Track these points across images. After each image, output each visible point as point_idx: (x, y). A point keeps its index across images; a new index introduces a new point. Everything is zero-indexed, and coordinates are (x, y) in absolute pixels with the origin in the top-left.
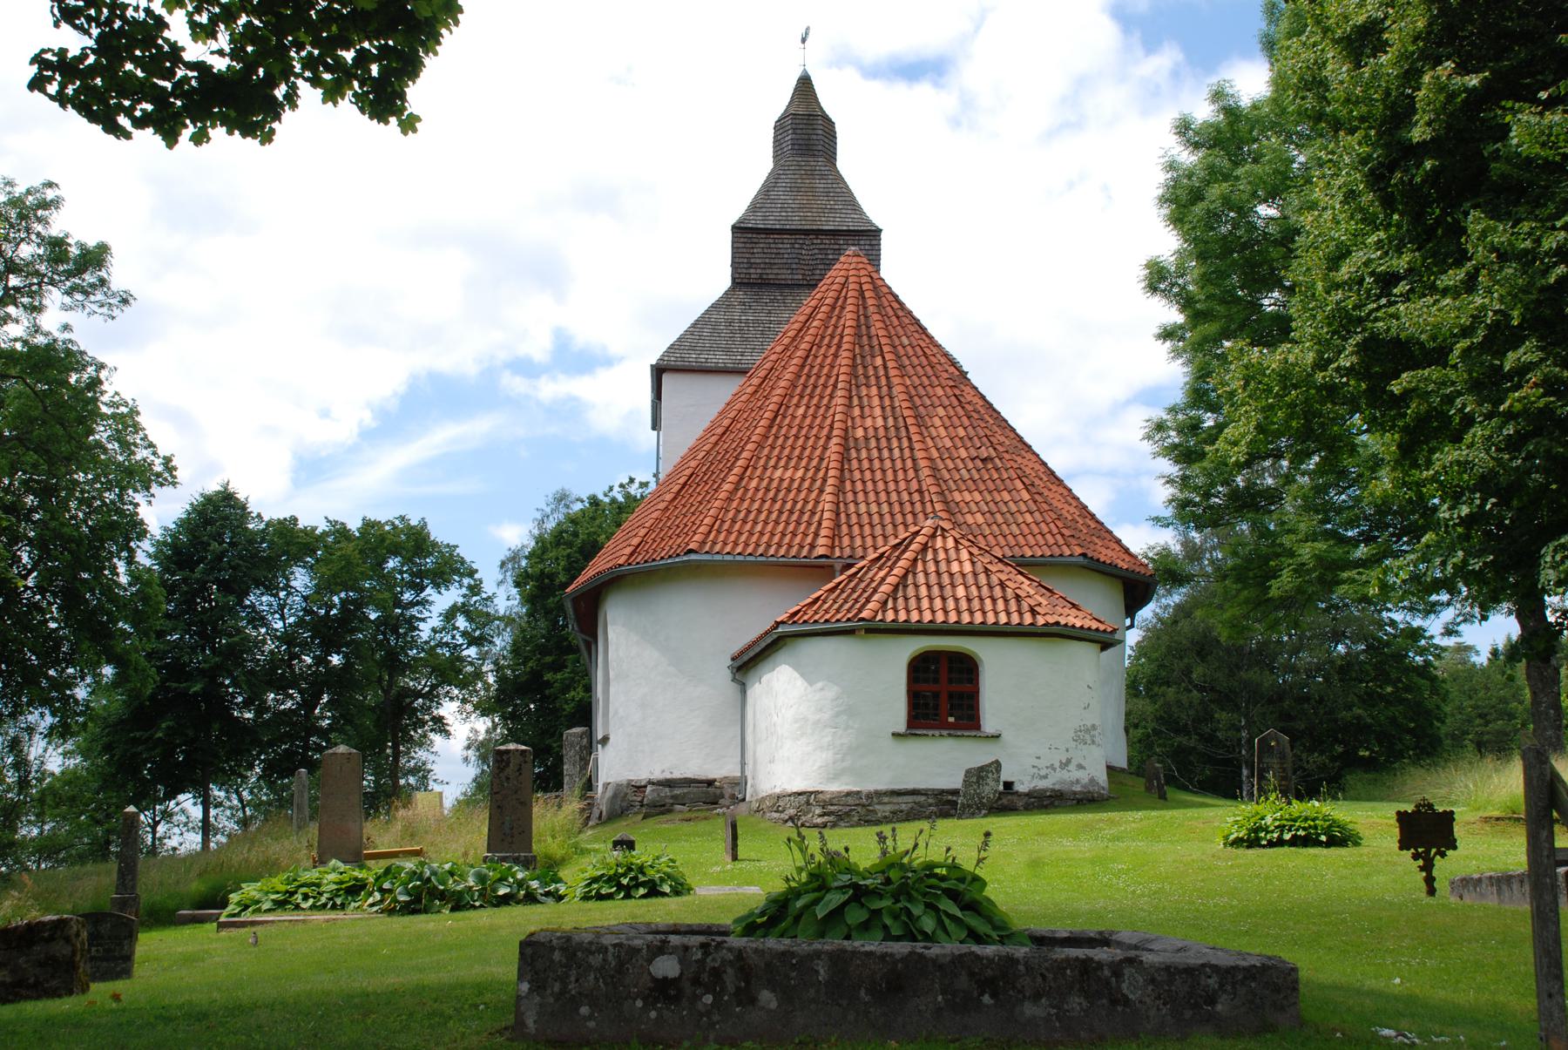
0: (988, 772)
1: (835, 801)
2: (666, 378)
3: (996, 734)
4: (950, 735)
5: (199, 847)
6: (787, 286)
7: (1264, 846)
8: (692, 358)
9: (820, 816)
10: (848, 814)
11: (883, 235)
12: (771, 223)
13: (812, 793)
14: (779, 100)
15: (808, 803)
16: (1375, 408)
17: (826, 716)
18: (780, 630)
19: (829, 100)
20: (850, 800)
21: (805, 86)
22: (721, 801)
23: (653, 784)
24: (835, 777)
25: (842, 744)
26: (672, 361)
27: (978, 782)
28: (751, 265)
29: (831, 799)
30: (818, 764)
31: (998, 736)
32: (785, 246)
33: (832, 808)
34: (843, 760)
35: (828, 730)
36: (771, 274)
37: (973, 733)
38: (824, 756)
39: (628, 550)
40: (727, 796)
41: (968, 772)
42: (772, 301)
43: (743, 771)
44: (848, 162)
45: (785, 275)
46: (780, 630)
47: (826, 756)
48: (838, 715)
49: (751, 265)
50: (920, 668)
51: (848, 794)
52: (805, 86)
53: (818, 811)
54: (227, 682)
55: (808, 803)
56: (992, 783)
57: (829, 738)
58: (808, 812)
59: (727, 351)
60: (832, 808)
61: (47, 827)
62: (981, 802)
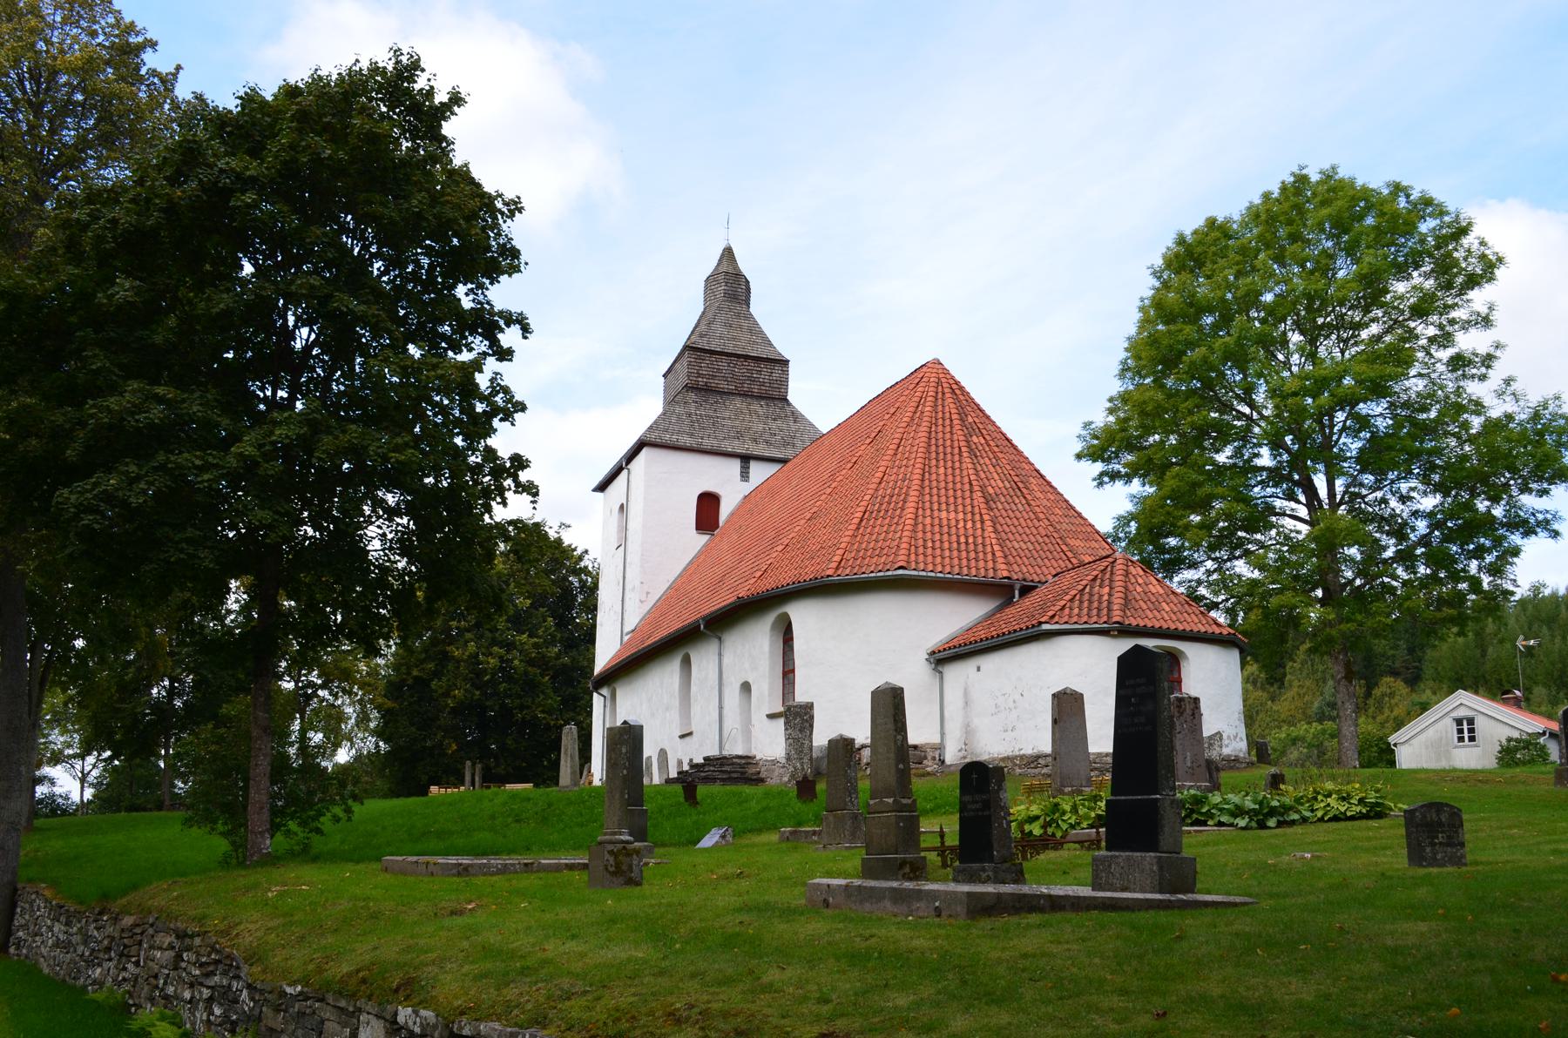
1: (1097, 760)
2: (645, 451)
5: (939, 845)
7: (60, 815)
12: (715, 345)
16: (1457, 403)
19: (745, 266)
21: (728, 253)
22: (925, 762)
26: (653, 437)
28: (699, 375)
32: (723, 364)
36: (713, 383)
39: (834, 565)
40: (929, 758)
42: (716, 402)
43: (943, 734)
44: (757, 308)
45: (723, 385)
49: (699, 375)
52: (728, 253)
54: (183, 769)
56: (1218, 749)
59: (692, 435)
61: (264, 206)
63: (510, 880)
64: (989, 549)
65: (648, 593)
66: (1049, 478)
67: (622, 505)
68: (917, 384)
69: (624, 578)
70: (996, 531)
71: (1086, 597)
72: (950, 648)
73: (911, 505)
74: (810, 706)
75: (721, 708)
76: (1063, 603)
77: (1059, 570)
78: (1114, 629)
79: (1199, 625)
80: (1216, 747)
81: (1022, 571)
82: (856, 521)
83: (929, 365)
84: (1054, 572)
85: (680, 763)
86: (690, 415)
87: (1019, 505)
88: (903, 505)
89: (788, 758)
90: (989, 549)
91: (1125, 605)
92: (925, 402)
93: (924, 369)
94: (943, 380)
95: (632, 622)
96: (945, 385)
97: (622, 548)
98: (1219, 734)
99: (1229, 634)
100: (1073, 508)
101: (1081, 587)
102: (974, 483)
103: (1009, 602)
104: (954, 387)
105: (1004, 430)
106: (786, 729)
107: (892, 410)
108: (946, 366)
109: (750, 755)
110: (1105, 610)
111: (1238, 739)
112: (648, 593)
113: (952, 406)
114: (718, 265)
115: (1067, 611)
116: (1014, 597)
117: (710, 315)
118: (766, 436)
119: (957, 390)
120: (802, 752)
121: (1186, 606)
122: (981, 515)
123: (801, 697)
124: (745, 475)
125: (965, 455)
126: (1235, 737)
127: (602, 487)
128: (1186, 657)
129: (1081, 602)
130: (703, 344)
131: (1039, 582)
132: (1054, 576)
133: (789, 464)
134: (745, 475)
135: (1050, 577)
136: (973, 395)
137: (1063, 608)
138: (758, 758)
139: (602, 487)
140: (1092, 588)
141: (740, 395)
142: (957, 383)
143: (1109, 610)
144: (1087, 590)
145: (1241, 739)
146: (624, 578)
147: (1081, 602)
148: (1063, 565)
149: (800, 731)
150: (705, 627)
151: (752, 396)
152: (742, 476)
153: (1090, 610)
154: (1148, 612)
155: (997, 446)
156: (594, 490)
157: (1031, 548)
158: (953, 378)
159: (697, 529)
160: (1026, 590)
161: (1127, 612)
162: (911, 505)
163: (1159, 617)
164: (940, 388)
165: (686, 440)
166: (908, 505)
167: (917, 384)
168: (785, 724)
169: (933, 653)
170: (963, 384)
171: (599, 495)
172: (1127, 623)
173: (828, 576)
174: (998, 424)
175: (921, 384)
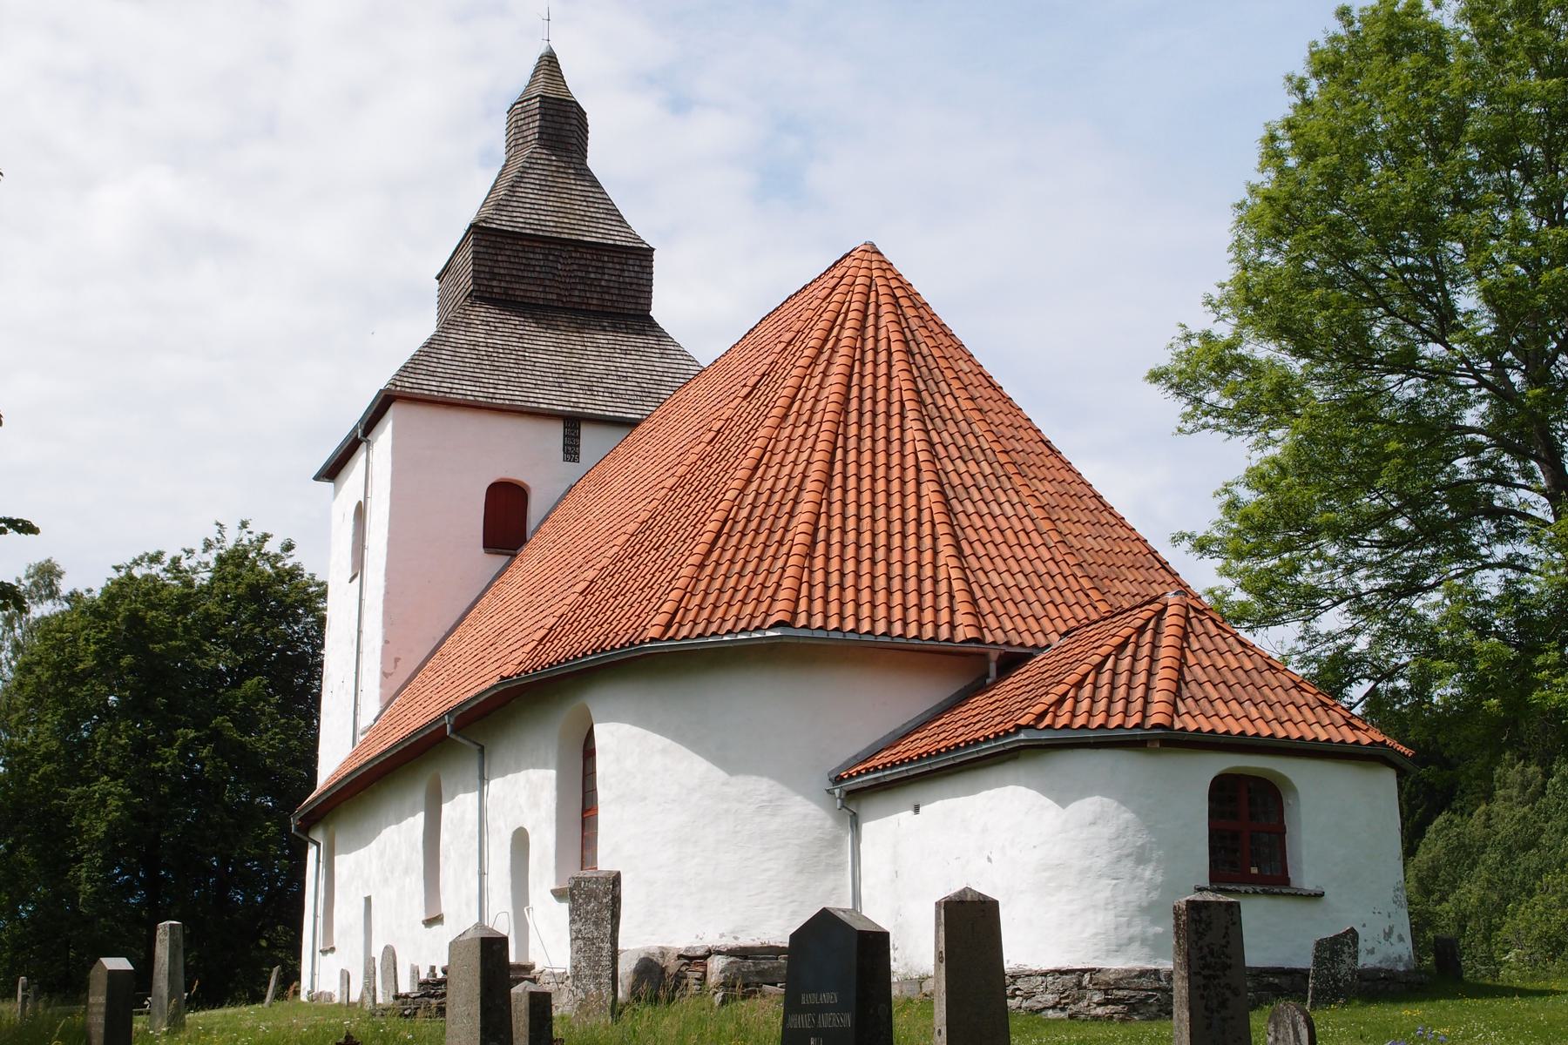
0: (1343, 944)
1: (1123, 984)
3: (1318, 891)
4: (1265, 893)
6: (537, 306)
8: (432, 386)
9: (1099, 1004)
10: (1143, 1001)
11: (656, 255)
13: (1084, 971)
14: (517, 76)
15: (1079, 985)
17: (1101, 862)
18: (1022, 736)
19: (580, 84)
20: (1144, 982)
21: (549, 63)
23: (719, 953)
24: (1119, 949)
25: (1127, 903)
26: (407, 385)
27: (1331, 959)
28: (494, 275)
29: (1116, 981)
30: (1090, 931)
31: (1319, 896)
33: (1120, 993)
34: (1129, 924)
35: (1105, 881)
37: (1284, 891)
38: (1100, 918)
39: (661, 619)
41: (1320, 945)
45: (536, 293)
46: (1022, 736)
47: (1103, 920)
48: (1119, 860)
49: (494, 275)
50: (1224, 791)
51: (1143, 973)
53: (1097, 997)
55: (1079, 985)
56: (1349, 961)
57: (1108, 893)
58: (1080, 999)
59: (476, 381)
60: (1120, 993)
62: (1337, 987)
63: (1444, 1008)
64: (943, 587)
65: (397, 660)
66: (1066, 455)
67: (360, 502)
68: (834, 289)
69: (359, 632)
70: (960, 554)
71: (1105, 678)
72: (902, 762)
73: (805, 508)
74: (616, 880)
75: (482, 874)
76: (1062, 689)
77: (1072, 623)
78: (1153, 739)
79: (1317, 728)
80: (1345, 957)
81: (1003, 630)
82: (708, 537)
83: (856, 254)
84: (1063, 629)
85: (415, 971)
86: (475, 346)
87: (1007, 506)
88: (793, 508)
89: (576, 975)
90: (943, 587)
91: (1178, 693)
92: (845, 320)
93: (848, 262)
94: (880, 281)
95: (366, 720)
96: (881, 290)
97: (357, 580)
98: (1352, 935)
99: (1373, 743)
100: (1108, 509)
101: (1097, 659)
102: (924, 466)
103: (979, 687)
104: (899, 293)
105: (988, 369)
106: (572, 921)
107: (787, 336)
108: (888, 257)
109: (523, 963)
110: (1104, 702)
111: (1394, 939)
112: (397, 660)
113: (893, 327)
114: (531, 83)
115: (1068, 704)
116: (987, 676)
117: (513, 172)
118: (610, 381)
119: (905, 300)
120: (598, 963)
121: (1293, 691)
122: (933, 525)
123: (606, 861)
124: (571, 451)
125: (911, 415)
126: (1388, 935)
127: (333, 471)
128: (1293, 789)
129: (1095, 687)
130: (504, 223)
131: (1035, 646)
132: (1066, 634)
133: (639, 429)
134: (571, 451)
135: (1054, 637)
136: (935, 309)
137: (1062, 699)
138: (538, 968)
139: (333, 471)
140: (1117, 659)
141: (565, 309)
142: (905, 286)
143: (1146, 702)
144: (1109, 665)
145: (1401, 939)
146: (359, 632)
147: (1095, 687)
148: (1081, 615)
149: (595, 923)
150: (452, 732)
151: (587, 313)
152: (566, 452)
153: (1111, 701)
154: (1219, 705)
155: (972, 399)
156: (317, 478)
157: (1024, 584)
158: (898, 277)
159: (485, 546)
160: (1013, 660)
161: (1180, 704)
162: (805, 508)
163: (1240, 714)
164: (873, 294)
165: (467, 390)
166: (800, 508)
167: (834, 289)
168: (571, 911)
169: (838, 780)
170: (916, 288)
171: (327, 486)
172: (1178, 725)
173: (652, 640)
174: (978, 358)
175: (840, 289)
